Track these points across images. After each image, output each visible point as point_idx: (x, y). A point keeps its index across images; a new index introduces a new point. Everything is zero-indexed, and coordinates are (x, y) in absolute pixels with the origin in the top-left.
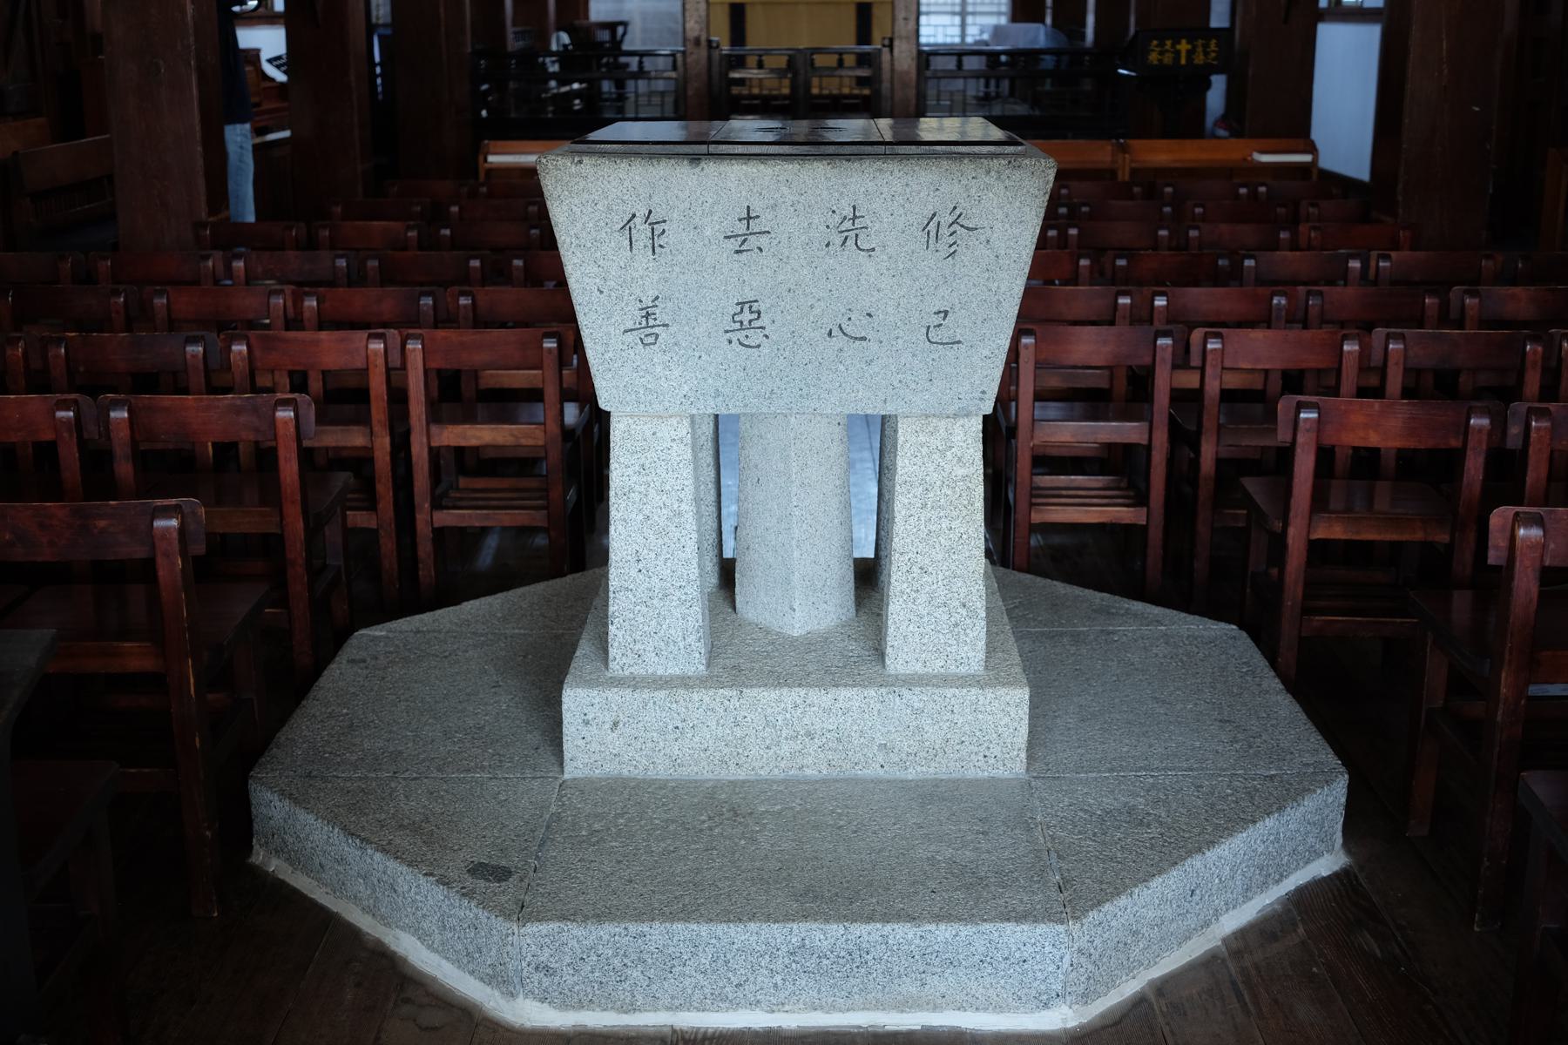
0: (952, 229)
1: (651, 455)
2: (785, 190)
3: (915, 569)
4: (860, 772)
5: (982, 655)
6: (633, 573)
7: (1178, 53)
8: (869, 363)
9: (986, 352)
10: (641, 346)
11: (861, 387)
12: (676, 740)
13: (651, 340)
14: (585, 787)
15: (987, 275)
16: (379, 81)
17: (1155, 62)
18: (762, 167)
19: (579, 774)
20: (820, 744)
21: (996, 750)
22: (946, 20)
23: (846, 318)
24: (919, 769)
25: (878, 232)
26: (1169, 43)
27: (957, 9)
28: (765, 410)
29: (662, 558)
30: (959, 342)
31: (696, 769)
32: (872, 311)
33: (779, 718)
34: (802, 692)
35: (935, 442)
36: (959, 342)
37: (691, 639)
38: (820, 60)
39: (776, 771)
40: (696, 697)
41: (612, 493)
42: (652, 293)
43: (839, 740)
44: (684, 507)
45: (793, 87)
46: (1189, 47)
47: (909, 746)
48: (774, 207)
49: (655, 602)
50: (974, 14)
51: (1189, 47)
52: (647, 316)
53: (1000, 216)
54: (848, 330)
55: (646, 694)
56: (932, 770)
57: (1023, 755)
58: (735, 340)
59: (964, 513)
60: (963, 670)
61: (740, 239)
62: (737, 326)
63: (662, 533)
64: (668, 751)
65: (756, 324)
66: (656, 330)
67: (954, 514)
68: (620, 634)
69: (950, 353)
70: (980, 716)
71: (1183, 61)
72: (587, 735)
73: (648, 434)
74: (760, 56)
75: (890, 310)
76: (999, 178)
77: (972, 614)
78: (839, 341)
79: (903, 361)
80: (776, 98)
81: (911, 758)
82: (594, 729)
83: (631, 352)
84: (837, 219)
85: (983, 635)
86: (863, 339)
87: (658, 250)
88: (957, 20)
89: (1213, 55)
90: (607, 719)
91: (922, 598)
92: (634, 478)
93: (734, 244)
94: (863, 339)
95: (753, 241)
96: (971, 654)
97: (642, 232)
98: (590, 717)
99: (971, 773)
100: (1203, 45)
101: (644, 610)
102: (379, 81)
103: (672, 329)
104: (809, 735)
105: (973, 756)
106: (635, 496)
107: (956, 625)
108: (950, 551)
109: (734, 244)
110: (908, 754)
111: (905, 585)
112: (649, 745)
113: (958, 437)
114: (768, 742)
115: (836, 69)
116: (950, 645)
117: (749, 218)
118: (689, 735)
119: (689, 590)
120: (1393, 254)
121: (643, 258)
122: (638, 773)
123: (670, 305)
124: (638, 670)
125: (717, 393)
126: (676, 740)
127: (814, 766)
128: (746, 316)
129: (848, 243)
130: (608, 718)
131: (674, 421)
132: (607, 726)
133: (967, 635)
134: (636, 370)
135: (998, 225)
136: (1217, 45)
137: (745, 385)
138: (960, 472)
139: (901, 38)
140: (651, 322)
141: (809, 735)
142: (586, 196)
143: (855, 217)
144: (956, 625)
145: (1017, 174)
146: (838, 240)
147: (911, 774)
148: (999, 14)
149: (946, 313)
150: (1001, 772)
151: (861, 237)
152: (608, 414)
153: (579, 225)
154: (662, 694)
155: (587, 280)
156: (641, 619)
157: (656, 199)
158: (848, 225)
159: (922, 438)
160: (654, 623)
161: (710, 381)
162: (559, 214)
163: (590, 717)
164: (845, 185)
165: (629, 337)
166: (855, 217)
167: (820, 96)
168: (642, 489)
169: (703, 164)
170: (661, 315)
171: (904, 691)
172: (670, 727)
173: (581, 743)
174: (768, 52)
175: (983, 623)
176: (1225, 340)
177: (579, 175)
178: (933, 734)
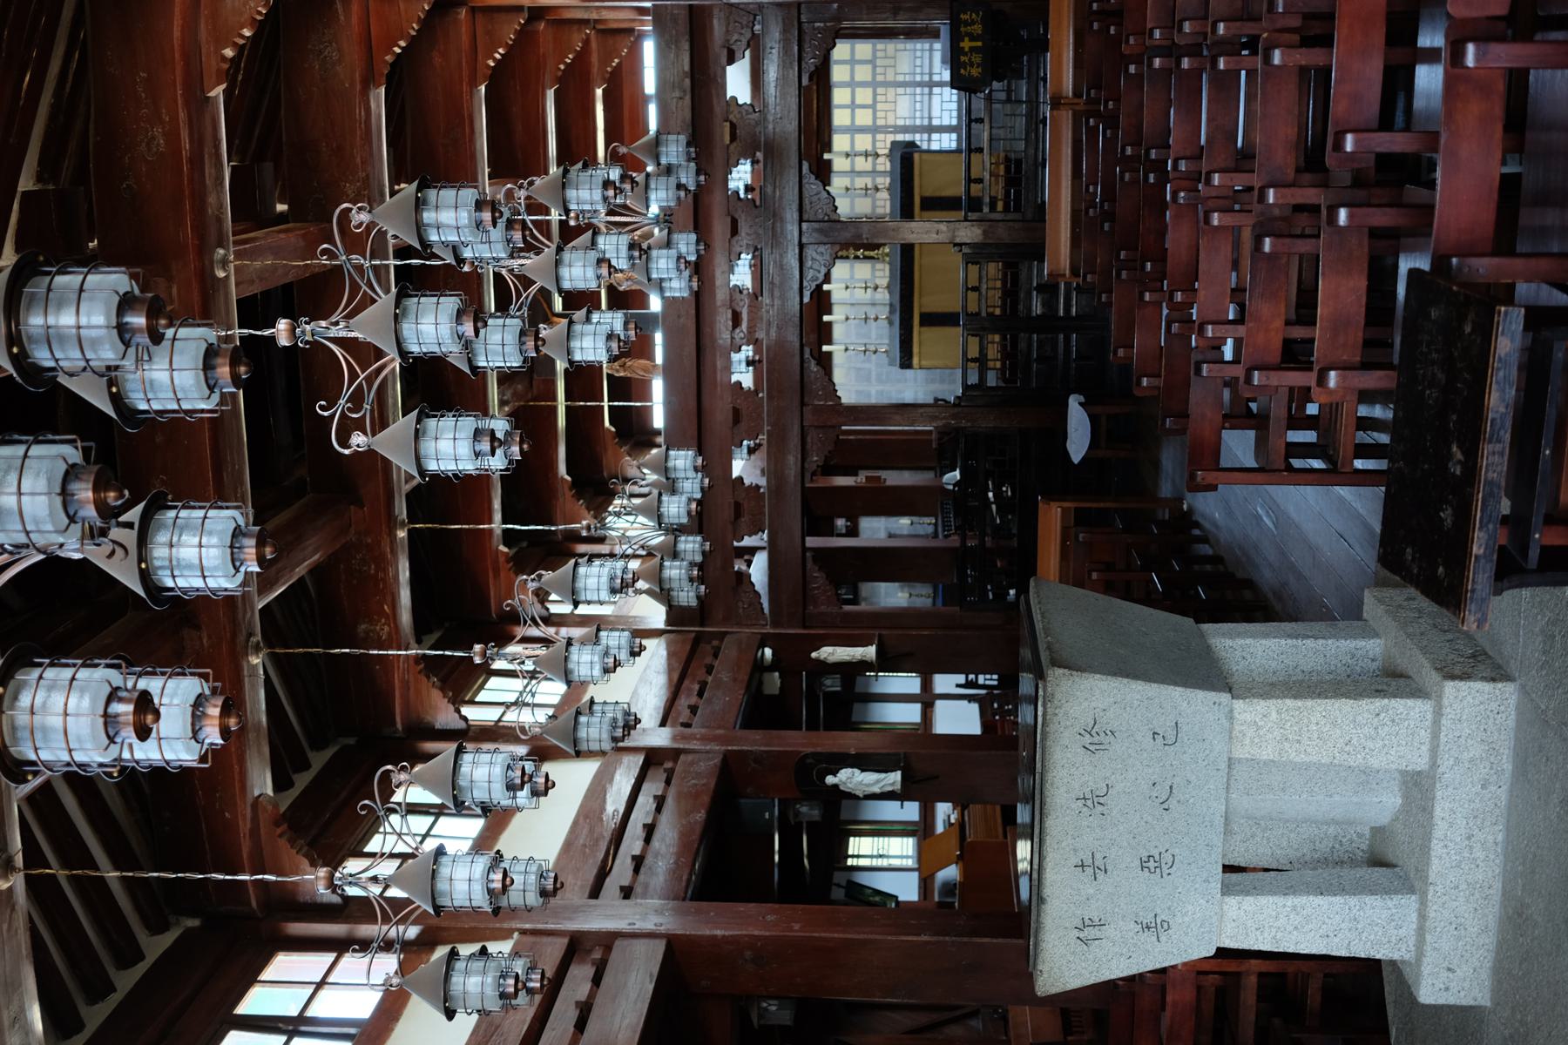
0: (1094, 734)
1: (1249, 923)
2: (1063, 844)
3: (1347, 749)
4: (1503, 802)
5: (1419, 702)
6: (1336, 940)
7: (972, 49)
8: (1189, 782)
9: (1185, 704)
10: (1170, 931)
11: (1207, 787)
12: (1466, 929)
13: (1165, 925)
14: (1496, 1003)
15: (1128, 709)
16: (994, 507)
17: (980, 70)
18: (1048, 859)
19: (1488, 996)
20: (1477, 830)
21: (1494, 706)
22: (936, 100)
23: (1156, 800)
24: (1504, 761)
25: (1095, 783)
26: (963, 58)
27: (926, 90)
28: (1220, 850)
29: (1327, 920)
30: (1176, 723)
31: (1491, 917)
32: (1151, 783)
33: (1454, 858)
34: (1435, 841)
35: (1251, 732)
36: (1176, 723)
37: (1390, 904)
38: (973, 379)
39: (1498, 861)
40: (1432, 915)
41: (1276, 950)
42: (1133, 925)
43: (1475, 817)
44: (1289, 903)
45: (995, 331)
46: (967, 39)
47: (1485, 768)
48: (1075, 850)
49: (1359, 926)
50: (931, 74)
51: (967, 39)
52: (1148, 928)
53: (1086, 704)
54: (1164, 798)
55: (1428, 948)
56: (1506, 752)
57: (1500, 685)
58: (1168, 871)
59: (1305, 713)
60: (1429, 716)
61: (1097, 871)
62: (1158, 870)
63: (1308, 919)
64: (1474, 936)
65: (1157, 858)
66: (1159, 922)
67: (1306, 721)
68: (1383, 952)
69: (1184, 728)
70: (1464, 717)
71: (979, 44)
72: (1457, 989)
73: (1234, 924)
74: (968, 289)
75: (1151, 771)
76: (1060, 707)
77: (1385, 709)
78: (1173, 803)
79: (1188, 760)
80: (1004, 347)
81: (1494, 766)
82: (1452, 985)
83: (1174, 937)
84: (1085, 809)
85: (1402, 701)
86: (1171, 787)
87: (1102, 922)
88: (936, 90)
89: (974, 16)
90: (1446, 975)
91: (1370, 744)
92: (1266, 935)
93: (1100, 875)
94: (1171, 787)
95: (1099, 862)
96: (1417, 710)
97: (1089, 933)
98: (1442, 986)
99: (1511, 723)
100: (965, 26)
101: (1365, 934)
102: (994, 507)
103: (1158, 911)
104: (1469, 838)
105: (1497, 722)
106: (1279, 935)
107: (1393, 721)
108: (1334, 724)
109: (1100, 875)
110: (1491, 768)
111: (1359, 756)
112: (1468, 947)
113: (1248, 717)
114: (1473, 866)
115: (980, 294)
116: (1409, 725)
117: (1082, 866)
118: (1463, 920)
119: (1352, 904)
120: (1149, 26)
121: (1108, 931)
122: (1490, 956)
123: (1141, 913)
124: (1412, 941)
125: (1206, 881)
126: (1466, 929)
127: (1495, 834)
128: (1152, 864)
129: (1102, 801)
130: (1446, 974)
131: (1225, 907)
132: (1451, 975)
133: (1402, 713)
134: (1187, 934)
135: (1094, 705)
136: (965, 13)
137: (1201, 863)
138: (1274, 715)
139: (954, 237)
140: (1153, 925)
141: (1469, 838)
142: (1063, 968)
143: (1084, 798)
144: (1393, 721)
145: (1058, 696)
146: (1100, 808)
147: (1508, 766)
148: (931, 50)
149: (1154, 733)
150: (1513, 701)
151: (1098, 793)
152: (1219, 949)
153: (1083, 971)
154: (1428, 937)
155: (1121, 966)
156: (1372, 937)
157: (1067, 925)
158: (1089, 803)
159: (1247, 741)
160: (1376, 929)
161: (1197, 886)
162: (1074, 983)
163: (1442, 986)
164: (1062, 807)
165: (1163, 938)
166: (1084, 798)
167: (1003, 307)
168: (1274, 930)
169: (1045, 896)
170: (1149, 918)
171: (1440, 770)
172: (1455, 933)
173: (1462, 994)
174: (965, 353)
175: (1393, 701)
176: (1206, 320)
177: (1049, 972)
178: (1477, 750)
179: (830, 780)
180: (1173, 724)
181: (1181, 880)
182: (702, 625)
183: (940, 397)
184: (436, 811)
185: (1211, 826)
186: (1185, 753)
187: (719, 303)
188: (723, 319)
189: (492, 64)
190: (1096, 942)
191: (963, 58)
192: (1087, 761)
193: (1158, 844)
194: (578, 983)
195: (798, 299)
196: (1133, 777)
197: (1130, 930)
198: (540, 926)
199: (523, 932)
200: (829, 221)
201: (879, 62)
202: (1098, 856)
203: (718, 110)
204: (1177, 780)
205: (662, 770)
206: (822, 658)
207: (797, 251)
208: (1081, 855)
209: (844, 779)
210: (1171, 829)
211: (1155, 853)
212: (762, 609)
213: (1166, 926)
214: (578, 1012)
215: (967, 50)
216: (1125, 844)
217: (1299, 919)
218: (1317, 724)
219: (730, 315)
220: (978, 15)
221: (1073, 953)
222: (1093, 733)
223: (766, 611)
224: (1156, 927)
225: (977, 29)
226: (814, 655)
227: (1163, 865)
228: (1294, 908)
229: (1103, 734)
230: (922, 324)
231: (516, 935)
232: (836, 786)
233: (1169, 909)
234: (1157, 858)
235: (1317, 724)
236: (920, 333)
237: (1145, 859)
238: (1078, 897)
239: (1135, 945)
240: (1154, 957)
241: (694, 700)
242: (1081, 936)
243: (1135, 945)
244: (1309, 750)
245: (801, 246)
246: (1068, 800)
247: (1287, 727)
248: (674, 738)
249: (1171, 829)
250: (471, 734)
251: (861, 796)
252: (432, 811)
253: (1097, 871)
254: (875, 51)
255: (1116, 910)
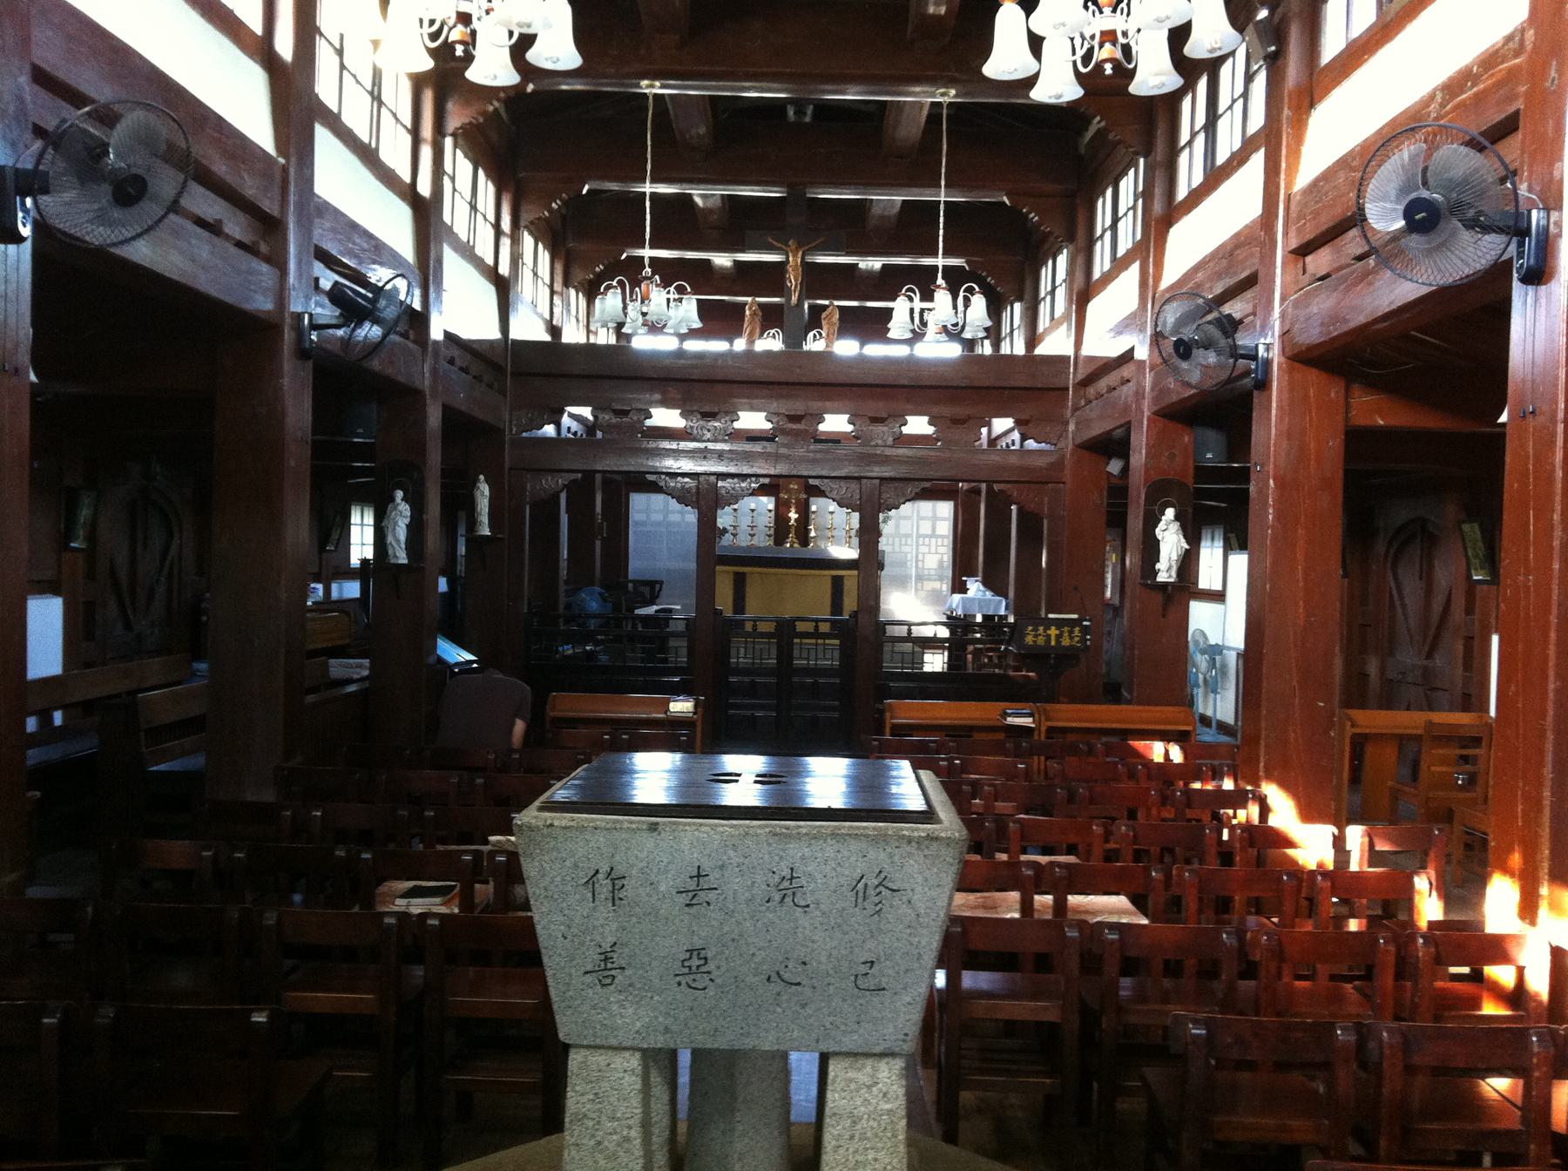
0: (878, 890)
8: (804, 1006)
9: (908, 999)
13: (608, 981)
15: (908, 931)
17: (1031, 643)
25: (813, 892)
30: (884, 989)
42: (611, 939)
46: (1057, 632)
51: (1057, 632)
52: (606, 959)
53: (920, 879)
54: (786, 976)
58: (683, 982)
59: (889, 1145)
61: (691, 894)
62: (687, 970)
65: (703, 969)
66: (613, 972)
71: (1053, 643)
75: (823, 959)
78: (777, 986)
83: (590, 991)
87: (617, 902)
93: (684, 899)
94: (799, 984)
95: (702, 896)
103: (628, 972)
109: (684, 899)
117: (699, 876)
121: (604, 911)
128: (695, 962)
135: (919, 889)
140: (609, 966)
146: (777, 897)
149: (872, 962)
151: (798, 895)
155: (552, 926)
157: (617, 858)
158: (786, 884)
161: (661, 1019)
164: (784, 851)
165: (589, 979)
174: (761, 619)
179: (399, 494)
180: (884, 985)
181: (670, 999)
182: (512, 374)
183: (664, 586)
184: (376, 93)
185: (742, 1034)
186: (844, 1000)
187: (810, 404)
188: (798, 407)
189: (1024, 210)
190: (590, 895)
191: (1041, 628)
192: (843, 880)
193: (723, 970)
194: (236, 226)
195: (814, 474)
196: (816, 938)
197: (603, 938)
198: (292, 188)
199: (285, 169)
200: (880, 504)
201: (933, 540)
202: (712, 895)
203: (815, 405)
204: (808, 991)
205: (406, 328)
206: (478, 484)
207: (856, 475)
208: (716, 874)
209: (400, 508)
210: (742, 985)
211: (711, 966)
212: (526, 431)
213: (606, 981)
214: (211, 221)
215: (1049, 632)
216: (726, 929)
217: (612, 1147)
218: (876, 1160)
219: (799, 413)
220: (1078, 642)
221: (576, 866)
222: (881, 888)
223: (524, 434)
224: (606, 969)
225: (1066, 642)
226: (482, 477)
227: (692, 977)
228: (627, 1139)
229: (877, 900)
230: (736, 574)
231: (282, 160)
232: (392, 499)
233: (630, 985)
234: (703, 969)
235: (876, 1160)
236: (728, 572)
237: (703, 953)
238: (655, 870)
239: (582, 944)
240: (563, 968)
241: (458, 362)
242: (600, 876)
243: (582, 944)
244: (841, 1151)
245: (859, 478)
246: (793, 857)
247: (871, 1123)
248: (436, 343)
249: (742, 985)
250: (439, 138)
251: (383, 524)
252: (376, 89)
253: (691, 894)
254: (942, 537)
255: (634, 920)
